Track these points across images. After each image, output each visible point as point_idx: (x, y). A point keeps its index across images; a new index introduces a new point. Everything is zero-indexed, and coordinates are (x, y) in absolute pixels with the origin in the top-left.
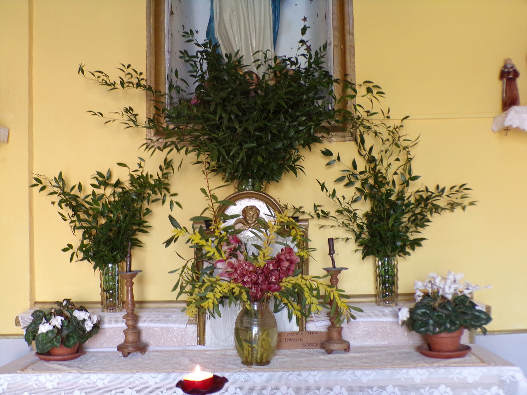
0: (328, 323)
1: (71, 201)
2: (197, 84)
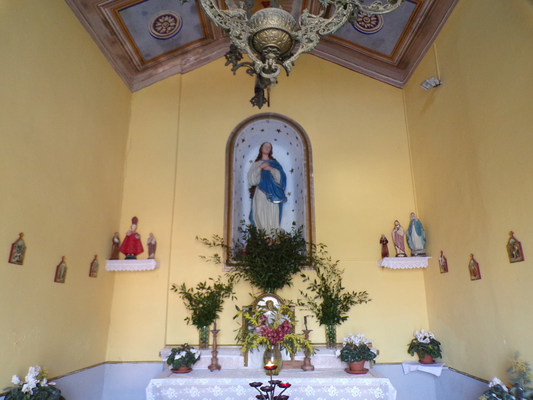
0: (304, 356)
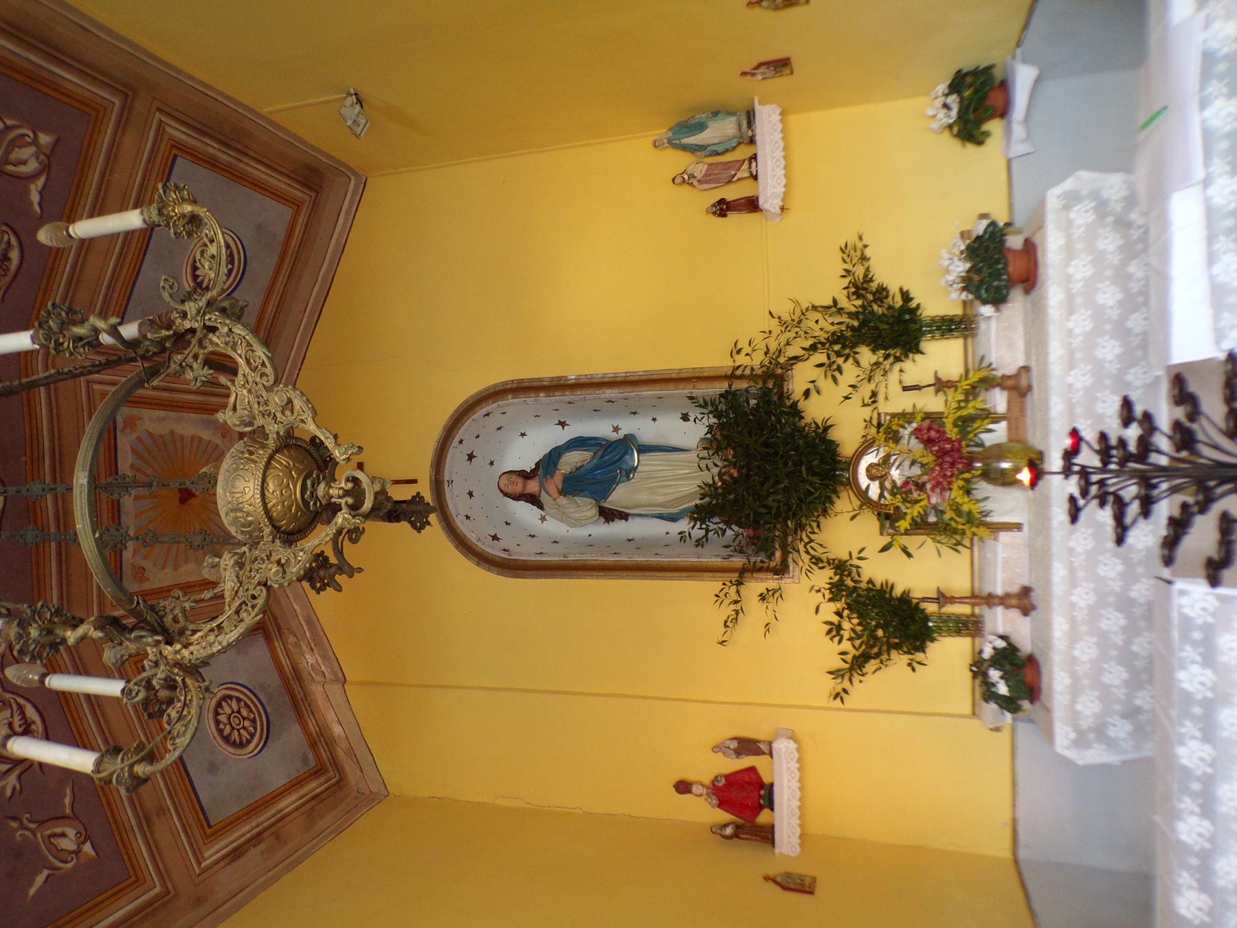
1: (858, 664)
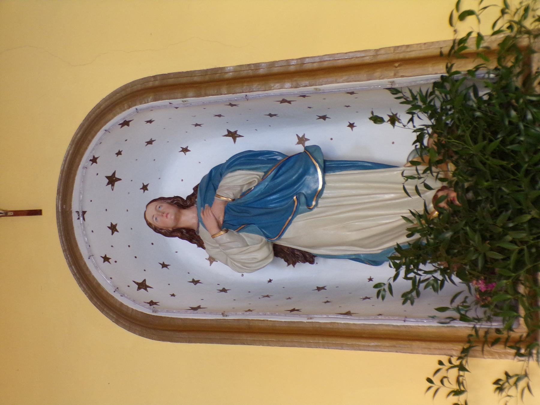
2: (456, 280)
